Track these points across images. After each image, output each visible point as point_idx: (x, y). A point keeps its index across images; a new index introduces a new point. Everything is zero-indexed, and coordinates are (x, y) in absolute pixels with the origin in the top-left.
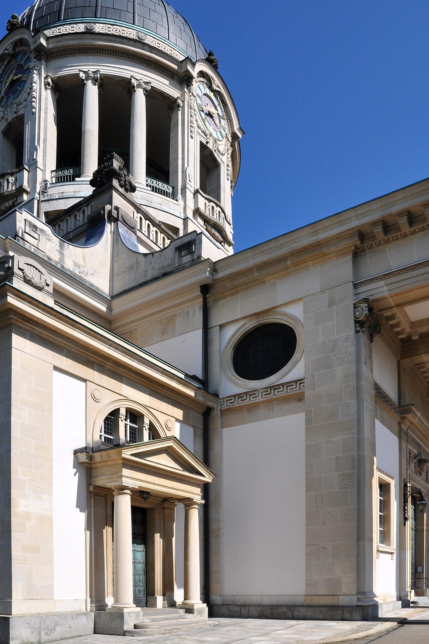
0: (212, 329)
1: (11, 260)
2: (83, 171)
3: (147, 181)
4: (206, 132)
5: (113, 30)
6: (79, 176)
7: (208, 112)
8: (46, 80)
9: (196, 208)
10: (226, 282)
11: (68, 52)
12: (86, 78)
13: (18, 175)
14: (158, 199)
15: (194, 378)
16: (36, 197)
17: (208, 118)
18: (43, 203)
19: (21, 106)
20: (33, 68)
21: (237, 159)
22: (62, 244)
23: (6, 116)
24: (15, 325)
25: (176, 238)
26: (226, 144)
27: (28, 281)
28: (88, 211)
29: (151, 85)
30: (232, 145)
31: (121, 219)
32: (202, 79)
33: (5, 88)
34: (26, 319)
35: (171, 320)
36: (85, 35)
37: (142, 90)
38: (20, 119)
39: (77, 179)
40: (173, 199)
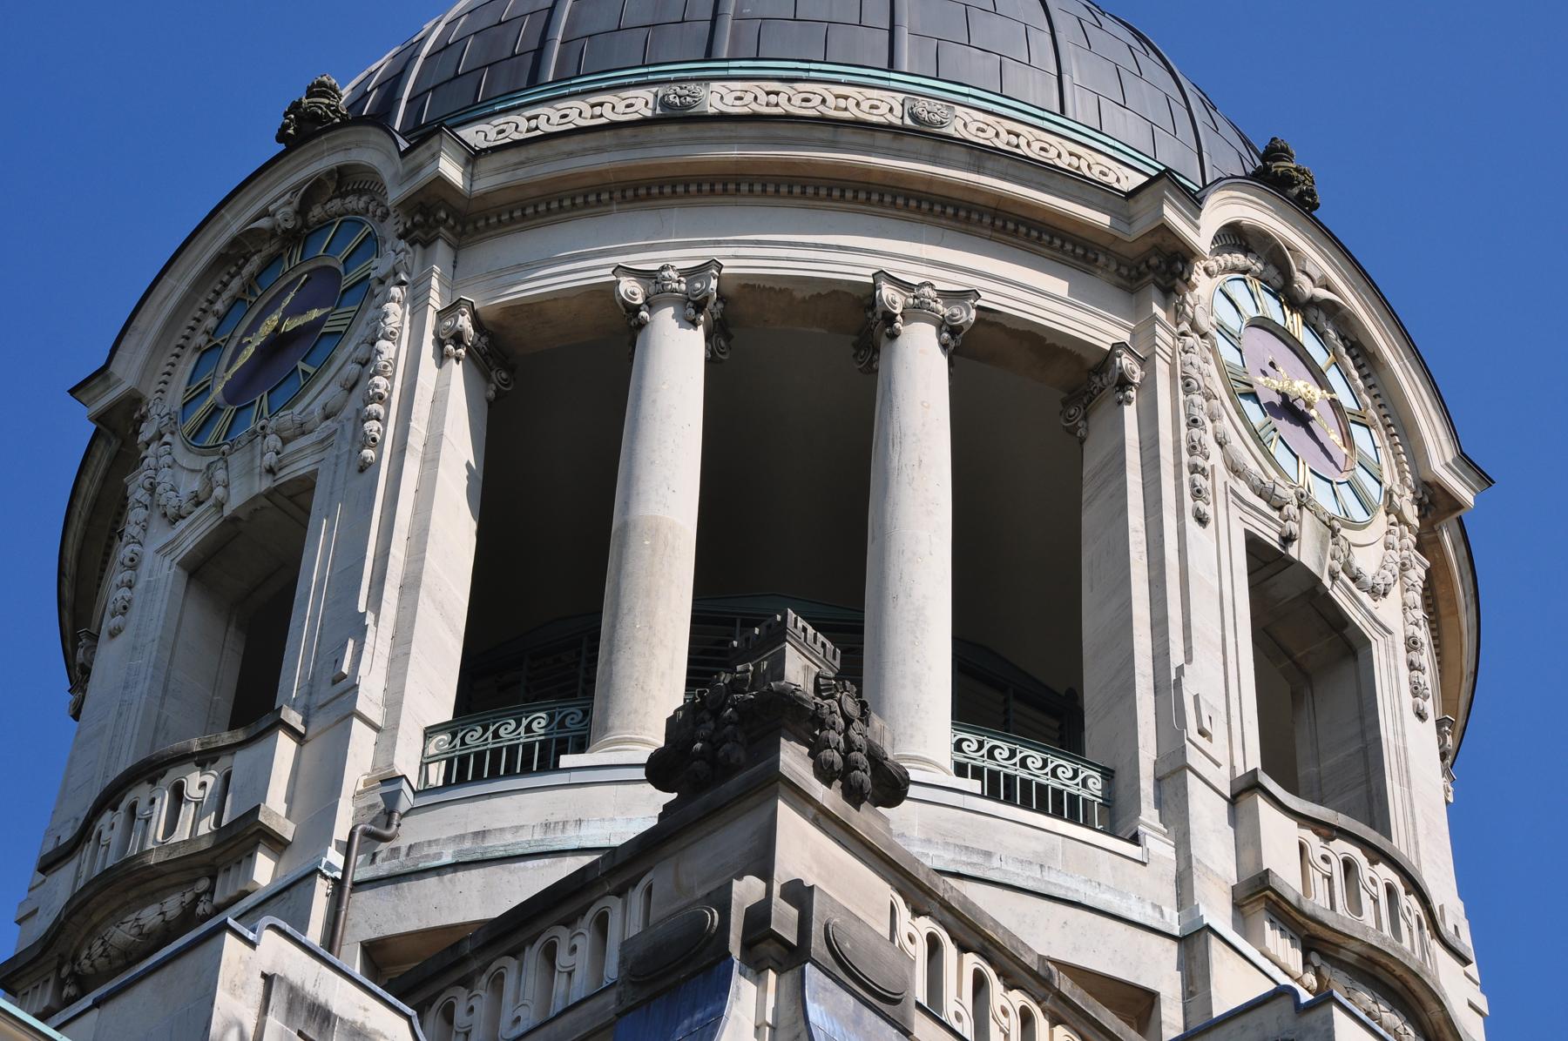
3: (958, 746)
4: (1278, 491)
5: (790, 100)
6: (581, 747)
7: (1277, 400)
9: (1251, 872)
11: (567, 203)
13: (240, 762)
14: (1020, 839)
16: (330, 866)
17: (1284, 426)
18: (363, 897)
20: (387, 276)
21: (1455, 612)
23: (219, 492)
26: (1393, 539)
28: (628, 919)
29: (979, 302)
30: (1426, 543)
31: (825, 951)
32: (1239, 259)
33: (235, 369)
37: (932, 329)
38: (290, 498)
39: (566, 761)
40: (1111, 832)
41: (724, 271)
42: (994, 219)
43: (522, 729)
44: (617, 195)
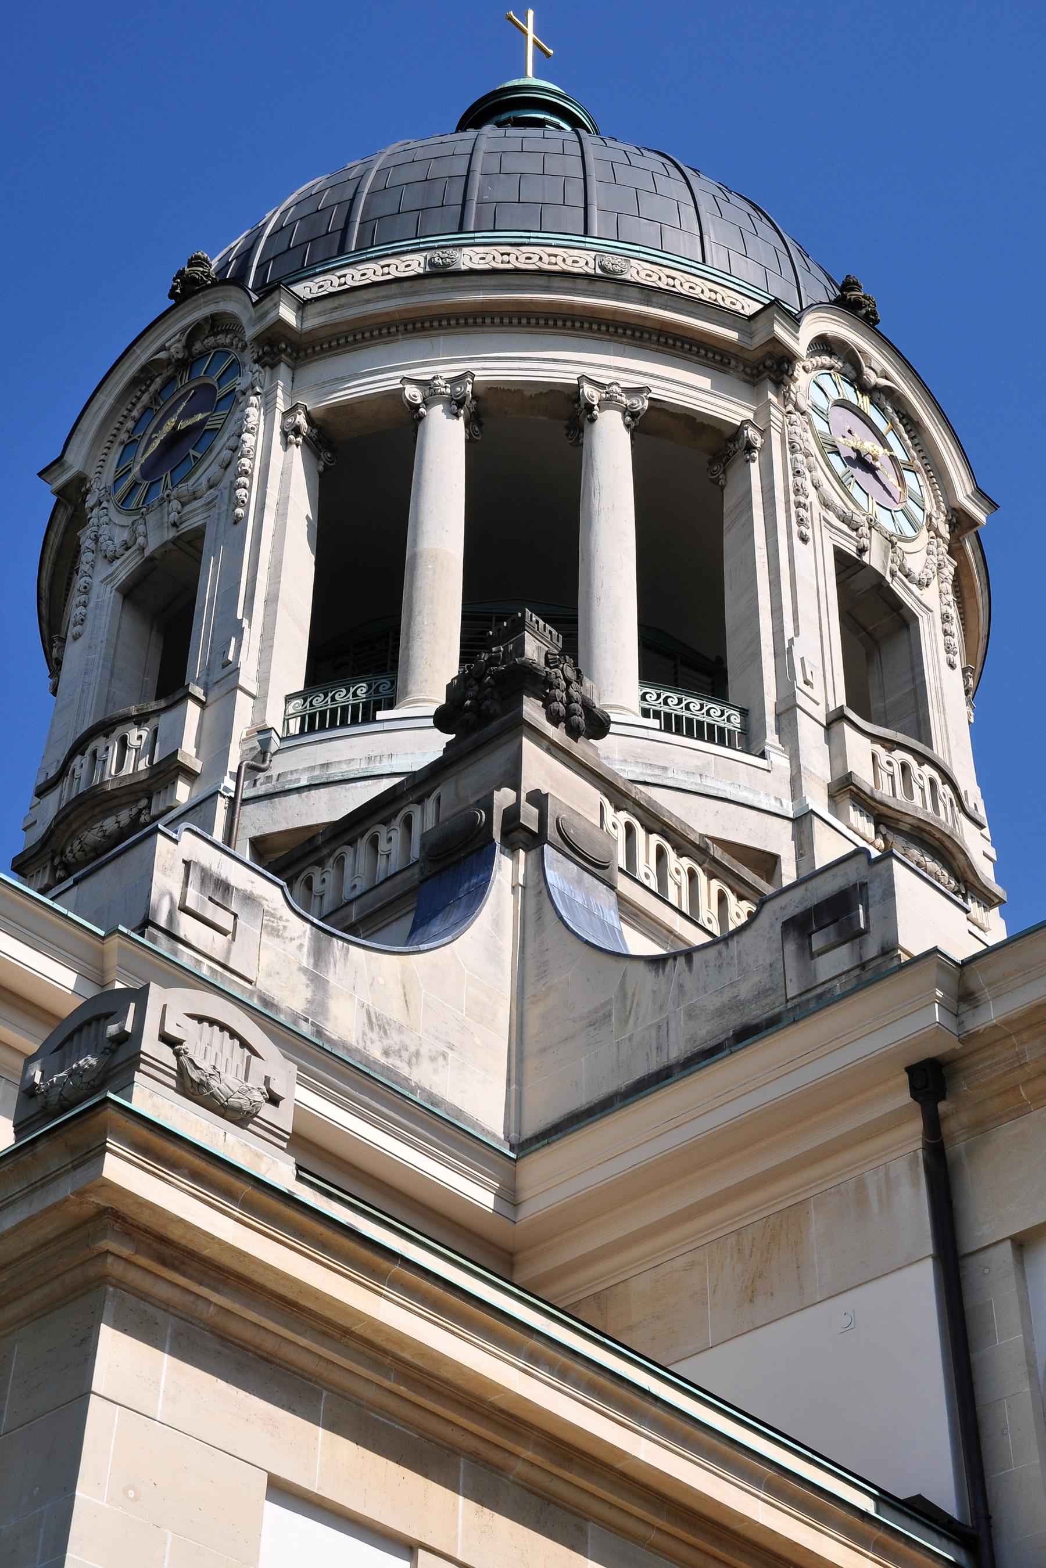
0: (981, 1257)
1: (132, 1006)
2: (405, 686)
3: (643, 697)
4: (855, 518)
5: (518, 259)
6: (390, 705)
7: (854, 455)
8: (290, 420)
9: (840, 774)
10: (1022, 1043)
11: (367, 335)
12: (424, 401)
13: (164, 721)
14: (687, 758)
15: (918, 1509)
16: (226, 789)
17: (858, 472)
18: (249, 808)
19: (196, 504)
20: (247, 389)
22: (324, 944)
23: (141, 540)
24: (120, 1284)
25: (768, 890)
26: (932, 548)
27: (192, 1088)
28: (425, 818)
29: (650, 395)
30: (955, 550)
32: (826, 360)
33: (147, 455)
34: (167, 1251)
35: (785, 1227)
36: (427, 281)
37: (619, 415)
38: (189, 543)
39: (380, 715)
41: (476, 379)
43: (350, 695)
44: (402, 328)
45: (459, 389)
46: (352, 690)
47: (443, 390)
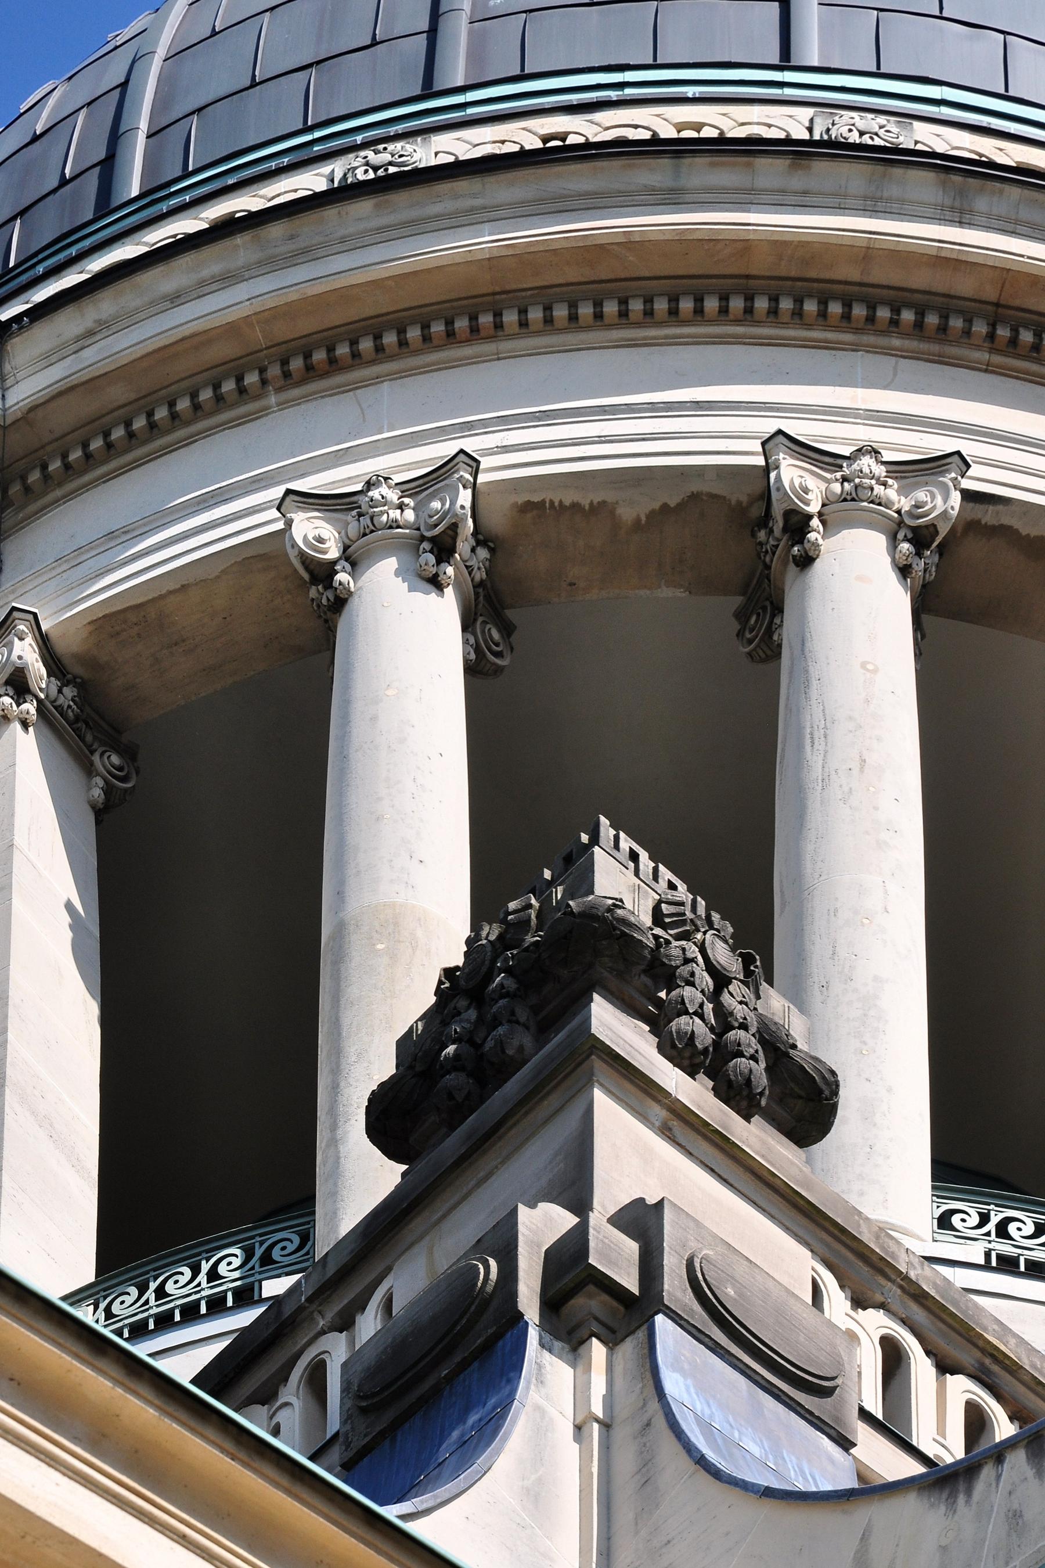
11: (183, 404)
29: (966, 484)
37: (880, 540)
41: (482, 478)
42: (993, 326)
43: (202, 1278)
44: (274, 371)
45: (436, 505)
46: (205, 1267)
47: (395, 514)
